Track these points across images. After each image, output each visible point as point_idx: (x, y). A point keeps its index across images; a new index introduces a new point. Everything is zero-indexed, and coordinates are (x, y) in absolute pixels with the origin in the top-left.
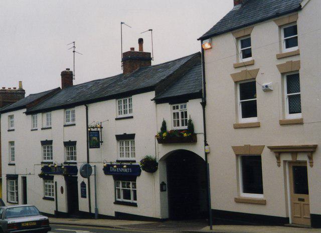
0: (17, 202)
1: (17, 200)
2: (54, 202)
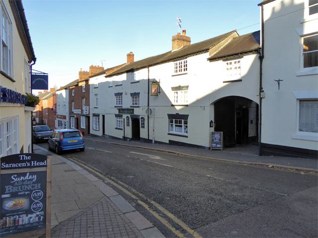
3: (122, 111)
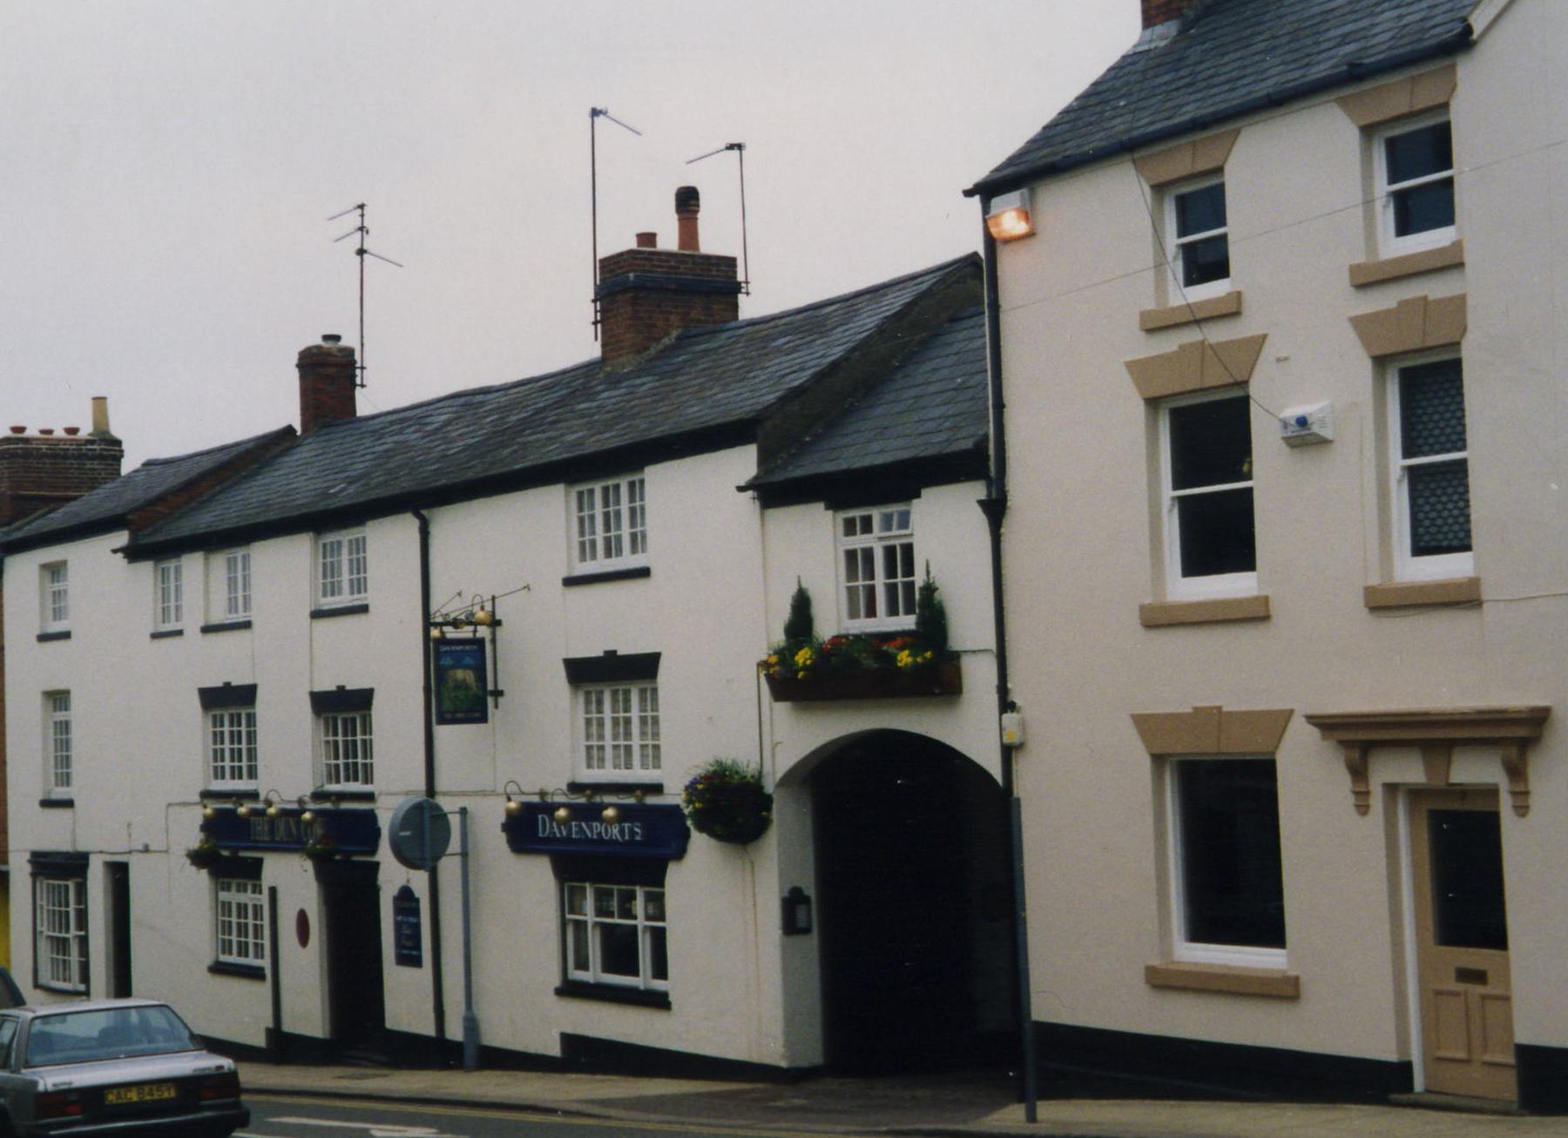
0: (82, 987)
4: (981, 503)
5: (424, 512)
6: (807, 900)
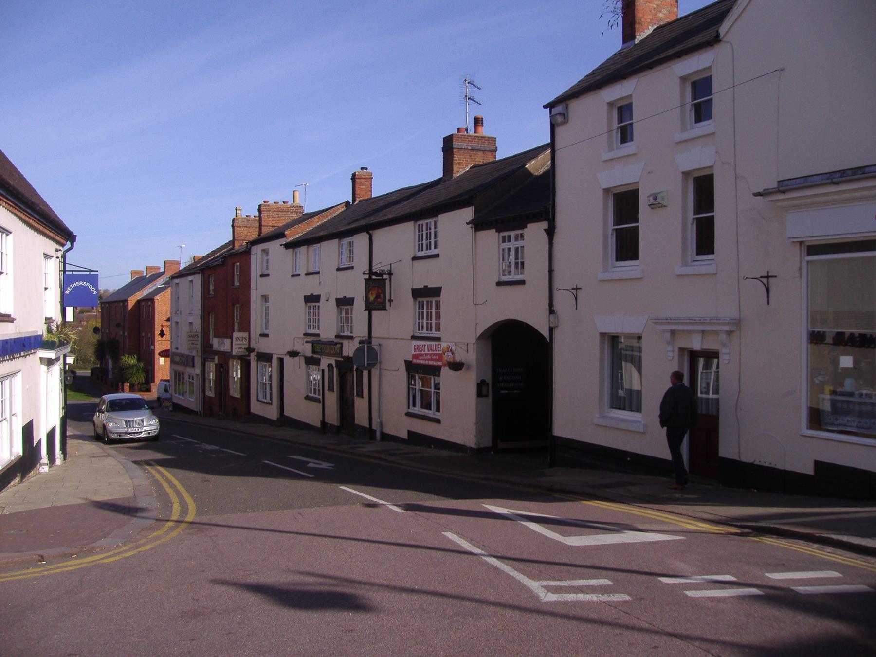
0: (270, 402)
1: (271, 399)
2: (321, 405)
3: (320, 347)
4: (545, 230)
5: (370, 232)
6: (488, 384)
